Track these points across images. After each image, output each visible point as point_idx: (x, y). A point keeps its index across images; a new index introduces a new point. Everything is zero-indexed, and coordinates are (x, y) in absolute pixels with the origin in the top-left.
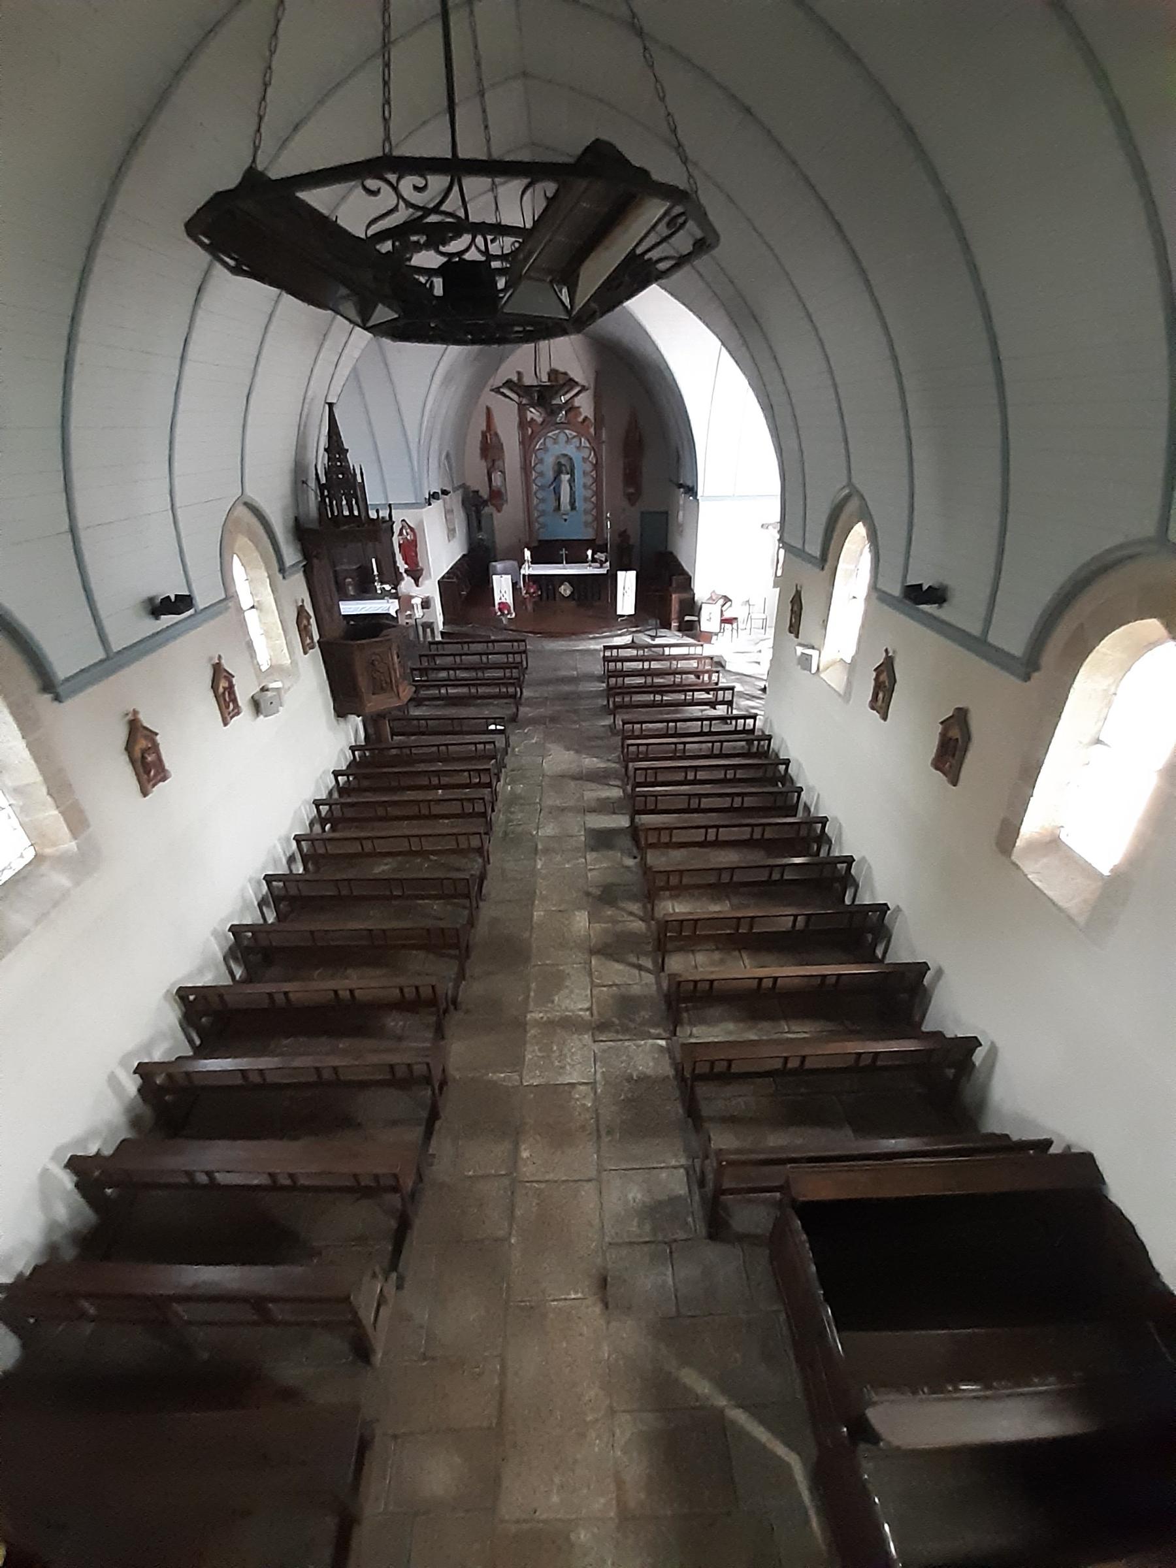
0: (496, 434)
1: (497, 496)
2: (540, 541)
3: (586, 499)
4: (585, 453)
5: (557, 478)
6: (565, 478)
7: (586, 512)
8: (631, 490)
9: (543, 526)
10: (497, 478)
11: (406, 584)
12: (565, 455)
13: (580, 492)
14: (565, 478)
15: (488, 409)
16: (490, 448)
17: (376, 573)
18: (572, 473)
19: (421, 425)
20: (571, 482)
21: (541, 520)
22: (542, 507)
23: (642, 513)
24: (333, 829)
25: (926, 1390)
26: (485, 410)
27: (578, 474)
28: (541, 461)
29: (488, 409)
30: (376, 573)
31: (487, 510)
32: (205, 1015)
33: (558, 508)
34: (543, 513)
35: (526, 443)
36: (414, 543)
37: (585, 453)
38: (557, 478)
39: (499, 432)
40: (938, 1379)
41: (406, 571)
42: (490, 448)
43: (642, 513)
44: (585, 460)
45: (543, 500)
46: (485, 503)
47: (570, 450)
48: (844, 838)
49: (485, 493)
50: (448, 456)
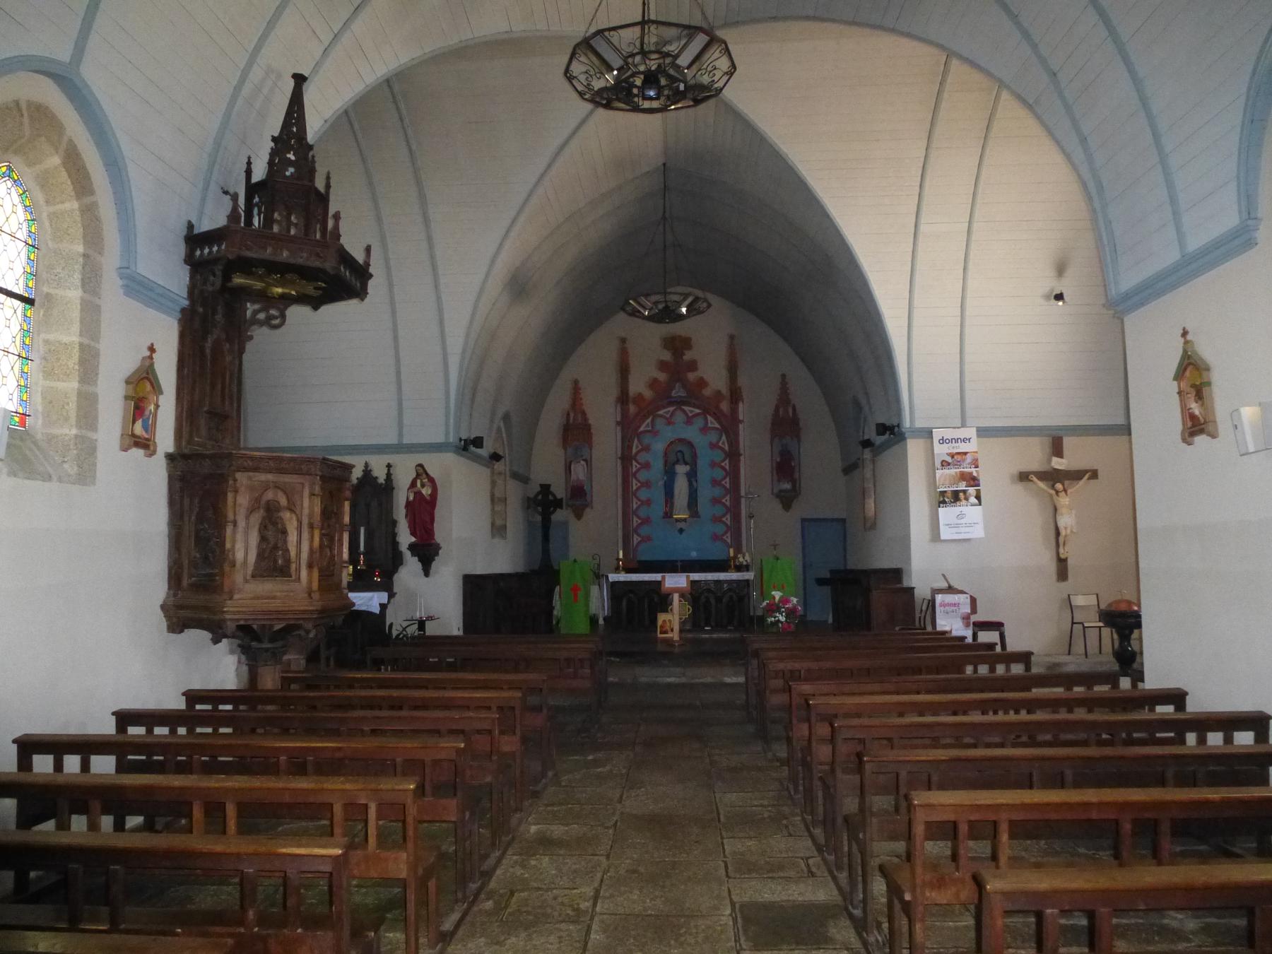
1: (579, 496)
4: (713, 437)
7: (717, 520)
8: (787, 486)
9: (647, 539)
10: (579, 471)
11: (410, 571)
12: (681, 440)
14: (682, 469)
15: (576, 382)
17: (362, 548)
18: (693, 464)
19: (493, 261)
20: (692, 476)
21: (645, 530)
23: (803, 520)
24: (149, 827)
27: (702, 463)
28: (646, 449)
30: (362, 548)
31: (559, 516)
33: (668, 515)
35: (628, 427)
36: (432, 502)
38: (670, 474)
40: (1168, 714)
41: (412, 547)
43: (803, 520)
44: (713, 446)
45: (648, 502)
46: (558, 504)
49: (559, 491)
50: (506, 418)
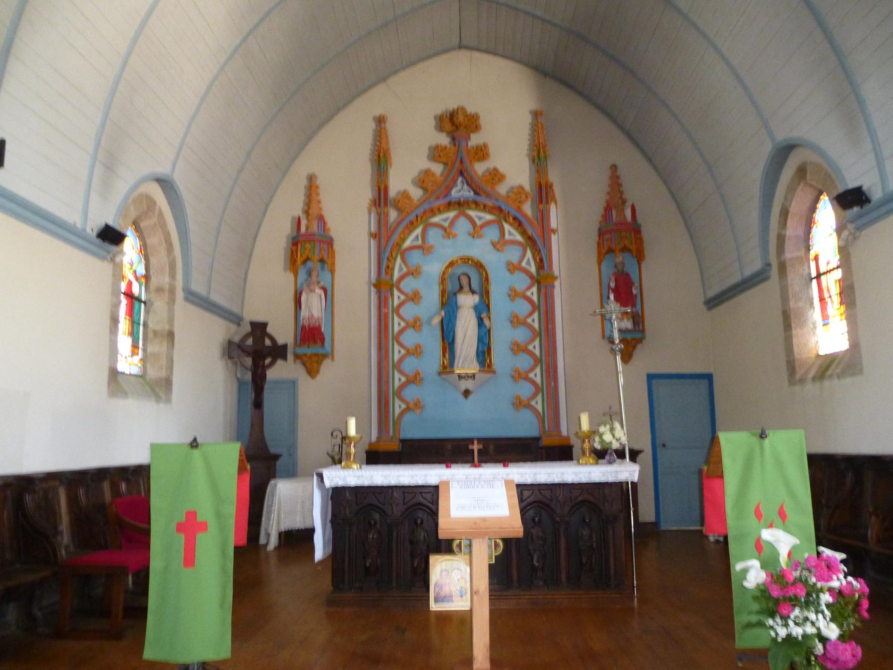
0: (321, 218)
2: (403, 441)
3: (517, 348)
5: (448, 304)
6: (467, 301)
7: (519, 376)
13: (503, 335)
14: (467, 301)
16: (309, 249)
18: (485, 294)
20: (483, 310)
21: (410, 393)
22: (410, 365)
23: (651, 377)
25: (819, 648)
26: (304, 182)
29: (311, 178)
32: (829, 367)
34: (415, 379)
35: (386, 244)
37: (513, 254)
38: (448, 304)
39: (326, 214)
42: (309, 249)
43: (651, 377)
44: (513, 268)
46: (279, 352)
47: (495, 262)
48: (595, 259)
49: (283, 331)
